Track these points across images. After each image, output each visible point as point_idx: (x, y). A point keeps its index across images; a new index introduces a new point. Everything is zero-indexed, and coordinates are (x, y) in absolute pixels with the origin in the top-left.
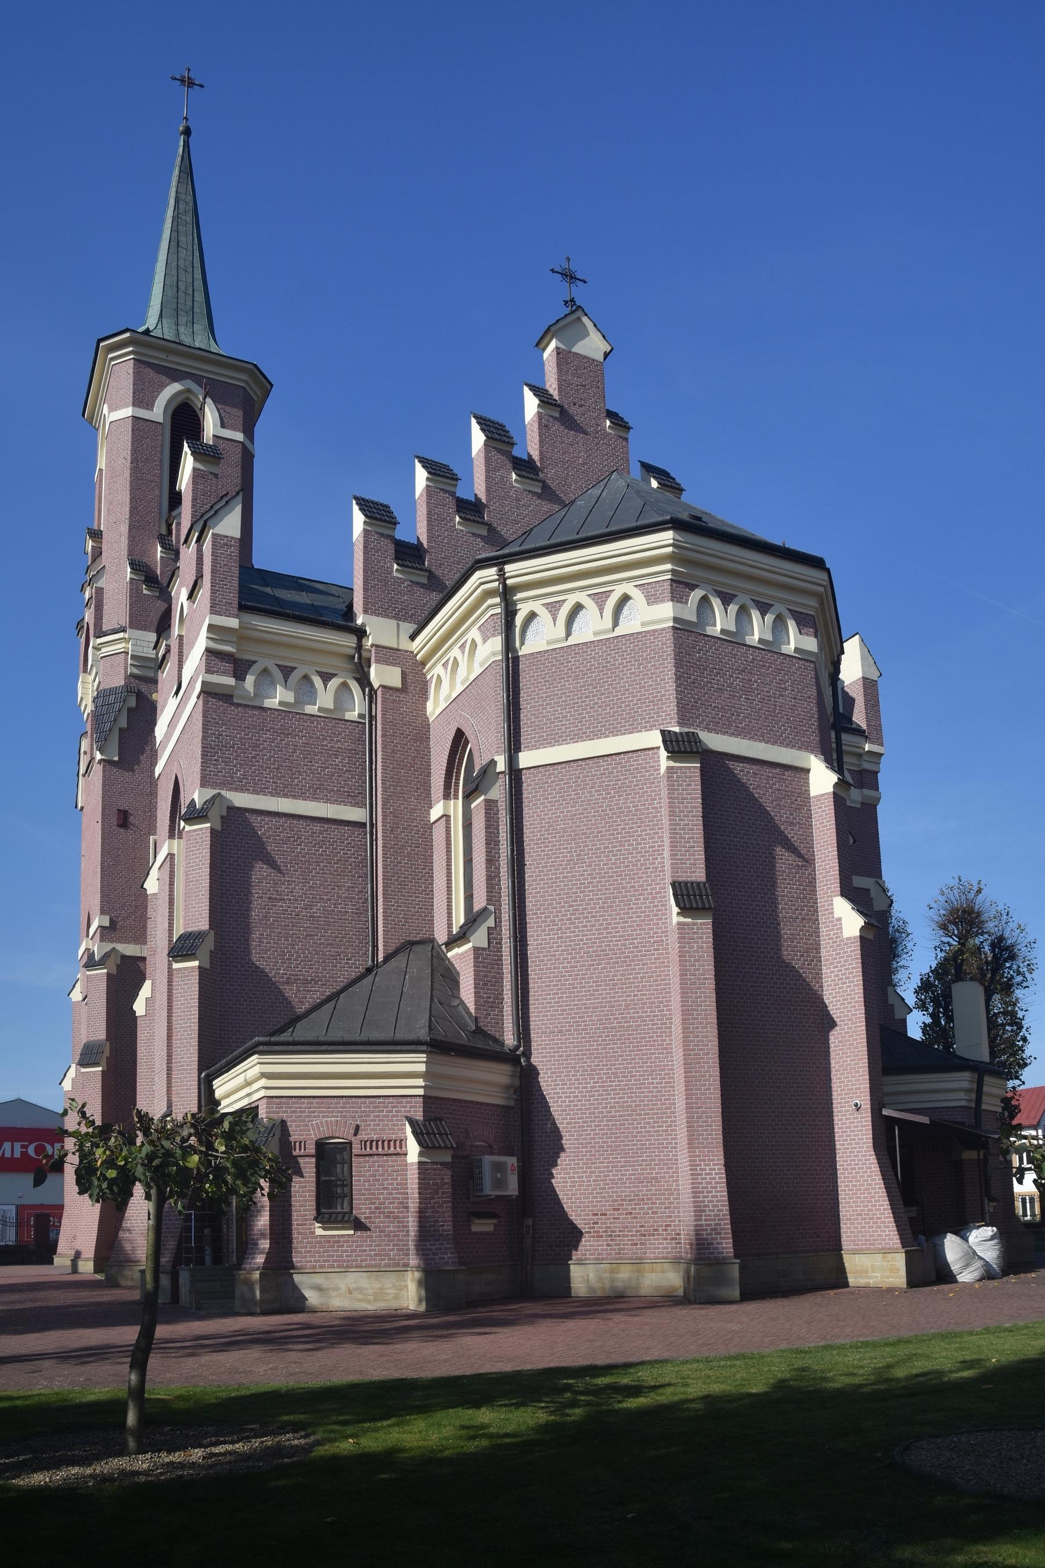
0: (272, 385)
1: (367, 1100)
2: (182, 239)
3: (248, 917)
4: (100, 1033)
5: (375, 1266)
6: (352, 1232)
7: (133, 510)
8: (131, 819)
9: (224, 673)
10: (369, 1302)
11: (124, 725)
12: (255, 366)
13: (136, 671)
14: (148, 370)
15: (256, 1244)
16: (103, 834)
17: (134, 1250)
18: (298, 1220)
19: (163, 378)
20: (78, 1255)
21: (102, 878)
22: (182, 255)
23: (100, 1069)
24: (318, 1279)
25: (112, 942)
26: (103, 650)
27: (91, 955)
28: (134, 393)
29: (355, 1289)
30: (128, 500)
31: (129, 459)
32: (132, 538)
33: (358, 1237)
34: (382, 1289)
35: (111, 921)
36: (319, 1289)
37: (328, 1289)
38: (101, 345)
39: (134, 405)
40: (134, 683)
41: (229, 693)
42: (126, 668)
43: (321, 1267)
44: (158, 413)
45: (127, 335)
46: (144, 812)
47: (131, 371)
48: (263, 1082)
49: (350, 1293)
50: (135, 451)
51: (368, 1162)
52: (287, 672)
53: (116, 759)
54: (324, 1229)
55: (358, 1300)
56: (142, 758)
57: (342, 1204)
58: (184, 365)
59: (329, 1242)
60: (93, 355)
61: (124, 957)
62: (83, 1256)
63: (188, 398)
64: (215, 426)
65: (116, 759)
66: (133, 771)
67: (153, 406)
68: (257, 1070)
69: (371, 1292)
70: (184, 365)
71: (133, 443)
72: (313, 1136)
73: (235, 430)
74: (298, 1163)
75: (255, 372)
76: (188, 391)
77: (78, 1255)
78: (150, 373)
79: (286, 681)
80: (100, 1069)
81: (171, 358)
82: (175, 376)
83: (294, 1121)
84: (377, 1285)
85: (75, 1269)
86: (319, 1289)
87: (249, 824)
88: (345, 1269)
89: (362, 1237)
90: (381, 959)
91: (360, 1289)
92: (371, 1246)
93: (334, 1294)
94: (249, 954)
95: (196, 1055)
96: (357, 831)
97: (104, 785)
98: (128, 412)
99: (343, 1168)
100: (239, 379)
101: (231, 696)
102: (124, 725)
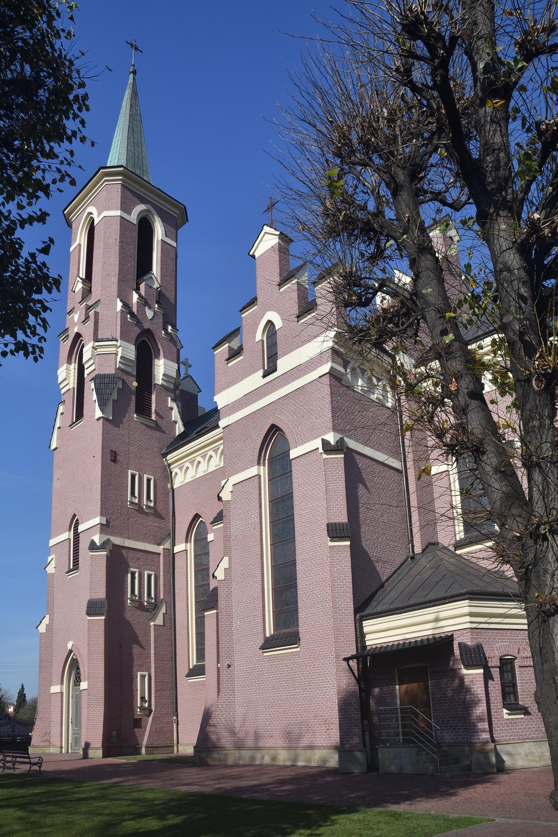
0: (188, 221)
1: (521, 632)
2: (135, 128)
3: (359, 517)
4: (101, 593)
5: (537, 738)
6: (522, 716)
7: (120, 270)
8: (118, 457)
9: (339, 364)
10: (536, 761)
11: (116, 398)
12: (185, 207)
13: (122, 366)
14: (128, 192)
15: (475, 726)
16: (102, 464)
17: (219, 739)
18: (494, 709)
19: (136, 200)
20: (87, 745)
21: (102, 492)
22: (136, 136)
23: (104, 618)
24: (509, 748)
25: (107, 535)
26: (98, 350)
27: (93, 543)
28: (121, 203)
29: (529, 753)
30: (118, 264)
31: (118, 240)
32: (119, 286)
33: (526, 719)
34: (542, 753)
35: (107, 521)
36: (509, 754)
37: (515, 754)
38: (101, 171)
39: (121, 210)
40: (120, 374)
41: (340, 377)
42: (116, 363)
43: (514, 739)
44: (133, 218)
45: (121, 169)
46: (125, 454)
47: (119, 190)
48: (468, 619)
49: (527, 756)
50: (121, 236)
51: (525, 671)
52: (363, 371)
53: (111, 418)
54: (509, 714)
55: (532, 761)
56: (124, 420)
57: (510, 699)
58: (145, 194)
59: (511, 723)
60: (92, 175)
61: (114, 545)
62: (91, 746)
63: (147, 215)
64: (162, 235)
65: (111, 418)
66: (119, 427)
67: (131, 213)
68: (467, 610)
69: (537, 755)
70: (145, 194)
71: (120, 231)
72: (498, 654)
73: (172, 239)
74: (490, 671)
75: (184, 210)
76: (148, 211)
77: (87, 745)
78: (130, 195)
79: (363, 376)
80: (104, 618)
81: (142, 190)
82: (143, 201)
83: (486, 644)
84: (540, 750)
85: (85, 756)
86: (509, 754)
87: (355, 460)
88: (523, 741)
89: (528, 719)
90: (418, 549)
91: (531, 753)
92: (532, 725)
93: (518, 757)
94: (361, 541)
95: (352, 603)
96: (397, 474)
97: (103, 434)
98: (118, 213)
99: (508, 675)
100: (175, 212)
101: (341, 379)
102: (116, 398)
